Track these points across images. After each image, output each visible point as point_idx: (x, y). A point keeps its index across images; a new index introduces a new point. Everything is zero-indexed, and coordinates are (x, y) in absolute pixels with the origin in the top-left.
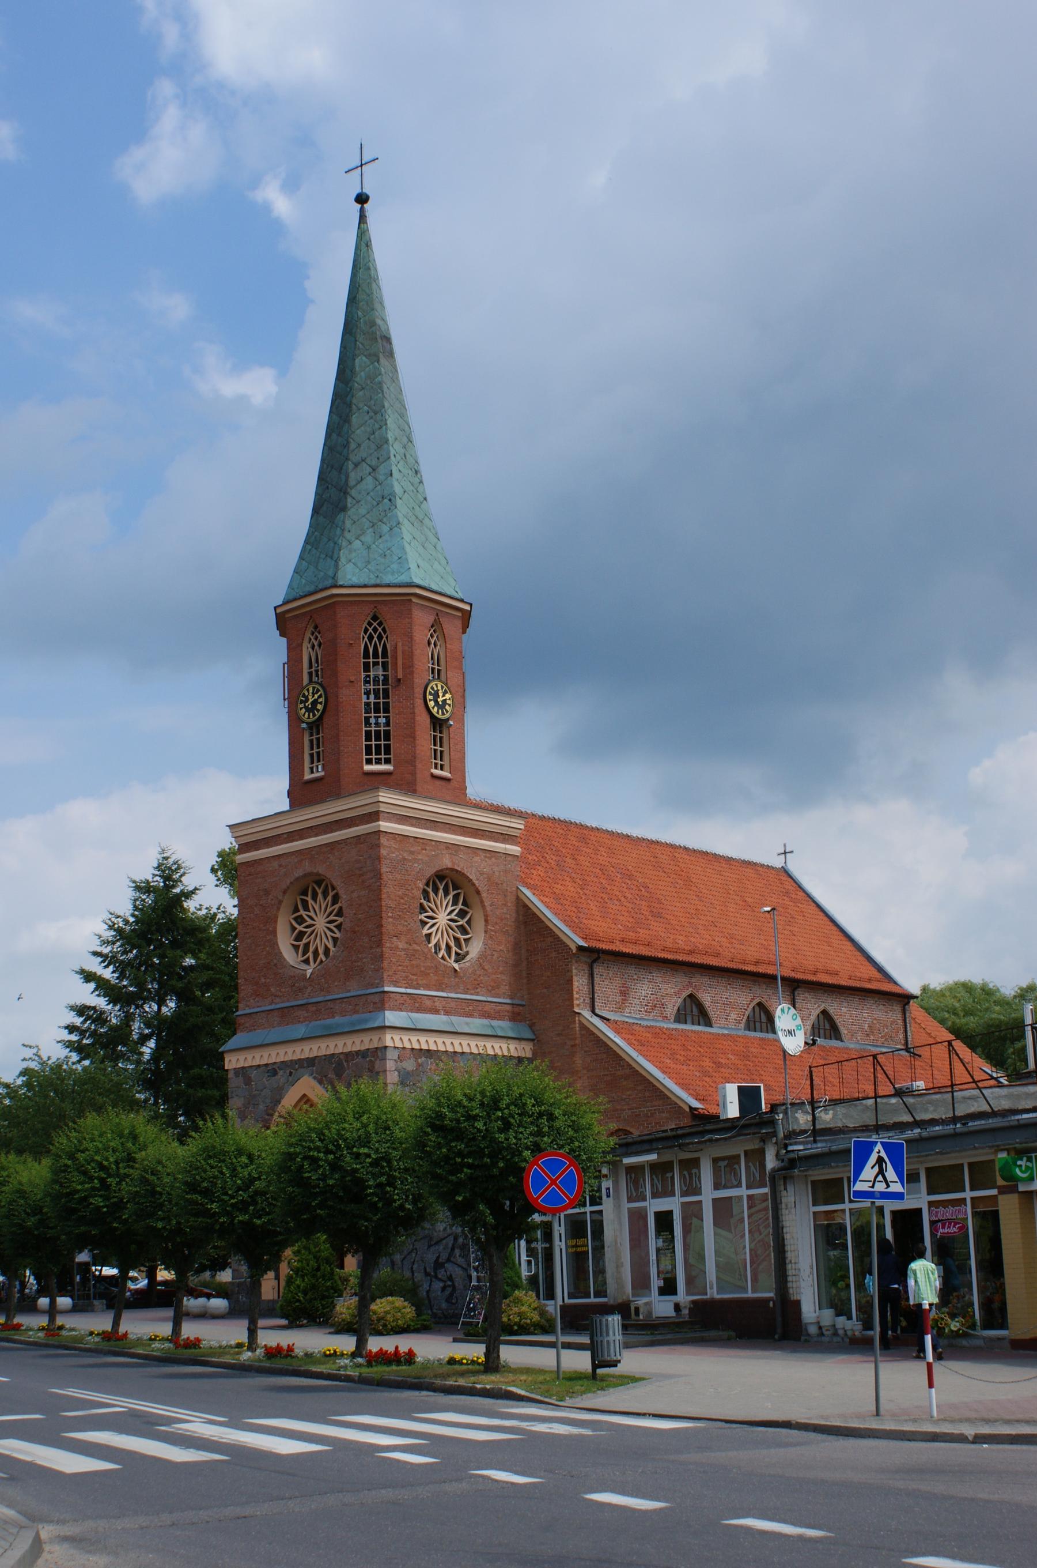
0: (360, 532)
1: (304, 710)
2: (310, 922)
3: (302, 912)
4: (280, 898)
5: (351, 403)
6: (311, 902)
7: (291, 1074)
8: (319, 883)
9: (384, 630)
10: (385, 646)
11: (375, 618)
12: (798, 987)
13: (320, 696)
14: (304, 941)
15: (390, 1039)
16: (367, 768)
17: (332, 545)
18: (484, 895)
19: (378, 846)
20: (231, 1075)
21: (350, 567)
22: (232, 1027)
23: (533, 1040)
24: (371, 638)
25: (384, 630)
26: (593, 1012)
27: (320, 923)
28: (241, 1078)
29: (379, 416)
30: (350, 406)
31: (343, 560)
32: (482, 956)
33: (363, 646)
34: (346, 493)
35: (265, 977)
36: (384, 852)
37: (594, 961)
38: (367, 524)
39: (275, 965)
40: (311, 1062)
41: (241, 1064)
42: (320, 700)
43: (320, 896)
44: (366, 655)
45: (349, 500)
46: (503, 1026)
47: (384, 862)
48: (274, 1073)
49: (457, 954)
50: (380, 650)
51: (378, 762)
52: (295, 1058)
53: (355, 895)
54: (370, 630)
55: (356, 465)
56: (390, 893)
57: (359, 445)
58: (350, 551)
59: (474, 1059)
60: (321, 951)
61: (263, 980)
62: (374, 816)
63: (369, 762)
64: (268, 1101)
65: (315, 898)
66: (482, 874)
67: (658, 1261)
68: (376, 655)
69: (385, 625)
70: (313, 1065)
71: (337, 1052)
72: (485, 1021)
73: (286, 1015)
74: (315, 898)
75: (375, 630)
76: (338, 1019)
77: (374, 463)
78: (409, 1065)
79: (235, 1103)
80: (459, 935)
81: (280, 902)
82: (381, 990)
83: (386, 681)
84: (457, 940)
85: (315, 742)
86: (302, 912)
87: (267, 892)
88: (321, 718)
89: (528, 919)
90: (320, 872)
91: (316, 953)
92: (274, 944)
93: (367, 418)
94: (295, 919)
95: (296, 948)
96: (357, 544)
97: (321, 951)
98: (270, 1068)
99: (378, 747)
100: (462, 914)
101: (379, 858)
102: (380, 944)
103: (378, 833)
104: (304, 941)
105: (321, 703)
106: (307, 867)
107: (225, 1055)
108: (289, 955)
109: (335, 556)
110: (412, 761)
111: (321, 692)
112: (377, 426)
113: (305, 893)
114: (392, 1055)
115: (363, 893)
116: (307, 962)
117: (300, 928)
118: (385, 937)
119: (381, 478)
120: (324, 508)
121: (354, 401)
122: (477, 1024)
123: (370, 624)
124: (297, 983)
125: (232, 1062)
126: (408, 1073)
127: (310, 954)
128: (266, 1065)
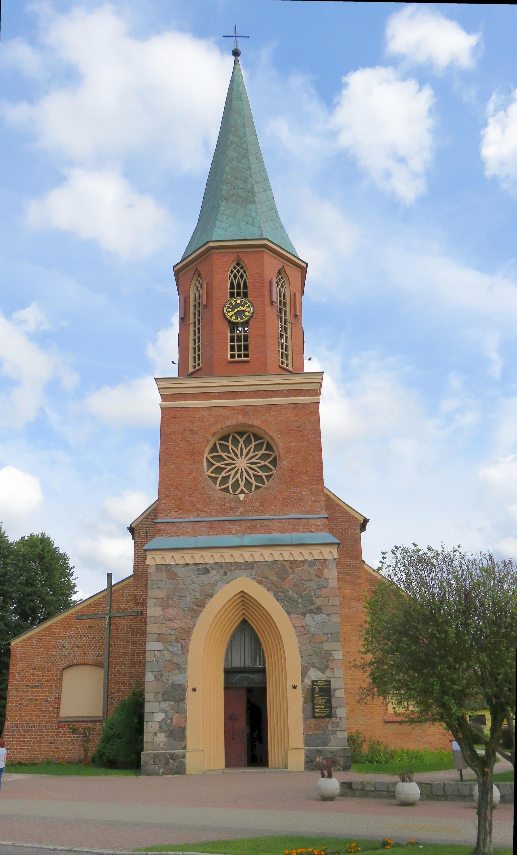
4: (210, 438)
7: (225, 573)
9: (245, 272)
11: (238, 264)
20: (152, 570)
23: (338, 544)
24: (235, 276)
25: (245, 272)
27: (242, 463)
33: (229, 282)
39: (203, 488)
40: (249, 566)
48: (206, 571)
50: (235, 284)
53: (293, 444)
64: (198, 595)
69: (245, 268)
70: (252, 568)
74: (235, 442)
75: (238, 271)
85: (197, 348)
87: (195, 433)
90: (255, 424)
104: (223, 474)
106: (241, 419)
123: (235, 268)
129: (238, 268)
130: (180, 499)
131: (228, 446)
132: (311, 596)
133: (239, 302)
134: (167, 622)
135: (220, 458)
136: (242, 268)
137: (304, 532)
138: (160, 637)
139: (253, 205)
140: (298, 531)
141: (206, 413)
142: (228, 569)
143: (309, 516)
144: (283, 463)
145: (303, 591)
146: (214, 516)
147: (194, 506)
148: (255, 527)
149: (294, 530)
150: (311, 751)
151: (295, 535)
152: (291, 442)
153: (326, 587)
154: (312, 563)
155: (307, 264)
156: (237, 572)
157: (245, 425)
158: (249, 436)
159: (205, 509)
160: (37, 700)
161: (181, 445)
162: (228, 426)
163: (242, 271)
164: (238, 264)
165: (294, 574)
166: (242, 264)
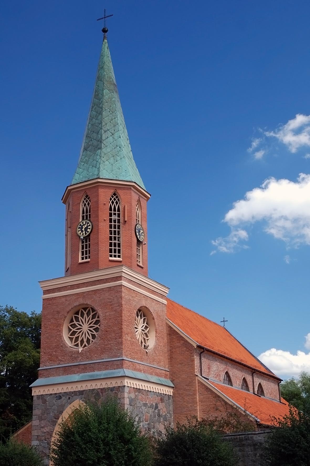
0: (108, 158)
2: (79, 327)
3: (75, 322)
4: (66, 315)
5: (102, 107)
6: (80, 317)
7: (69, 398)
8: (85, 309)
9: (118, 199)
10: (119, 207)
11: (115, 194)
12: (255, 372)
13: (89, 225)
14: (76, 336)
15: (127, 382)
16: (110, 258)
17: (95, 162)
18: (156, 320)
19: (121, 292)
21: (104, 171)
22: (35, 377)
23: (173, 387)
24: (113, 202)
25: (118, 199)
26: (201, 375)
27: (85, 327)
28: (40, 400)
29: (114, 113)
30: (102, 108)
31: (101, 168)
32: (155, 348)
34: (101, 142)
35: (56, 351)
36: (123, 295)
37: (201, 353)
38: (111, 155)
39: (62, 346)
40: (81, 393)
41: (42, 393)
42: (89, 227)
43: (85, 315)
44: (111, 209)
45: (103, 145)
46: (164, 380)
47: (123, 299)
48: (60, 398)
49: (145, 346)
50: (117, 208)
51: (115, 256)
52: (72, 391)
53: (108, 314)
54: (113, 199)
55: (105, 132)
56: (125, 314)
58: (104, 165)
59: (154, 395)
60: (85, 340)
62: (119, 278)
63: (111, 256)
64: (56, 412)
65: (82, 315)
66: (155, 311)
68: (115, 210)
69: (119, 197)
71: (96, 388)
72: (157, 377)
73: (67, 370)
74: (82, 315)
75: (115, 199)
76: (96, 373)
77: (113, 132)
78: (133, 396)
79: (36, 412)
80: (145, 337)
81: (65, 317)
82: (122, 358)
83: (119, 221)
84: (144, 339)
85: (85, 246)
86: (75, 322)
87: (58, 312)
88: (89, 235)
89: (172, 333)
90: (88, 303)
91: (82, 341)
92: (61, 337)
93: (109, 114)
94: (71, 326)
95: (71, 339)
96: (107, 163)
97: (85, 340)
98: (57, 395)
100: (146, 327)
101: (121, 297)
102: (121, 337)
103: (121, 286)
104: (76, 336)
105: (90, 229)
106: (81, 301)
107: (32, 389)
108: (68, 343)
109: (98, 166)
110: (131, 257)
111: (90, 223)
112: (113, 117)
113: (77, 313)
114: (126, 390)
115: (112, 313)
116: (77, 345)
117: (73, 330)
118: (123, 334)
119: (116, 138)
120: (90, 148)
121: (104, 106)
122: (154, 379)
124: (74, 356)
125: (35, 392)
126: (132, 399)
127: (79, 342)
128: (56, 394)
130: (51, 355)
134: (42, 429)
136: (117, 197)
138: (38, 438)
141: (63, 299)
142: (71, 396)
143: (113, 359)
146: (66, 364)
147: (57, 358)
148: (86, 368)
152: (106, 313)
154: (112, 389)
156: (75, 397)
163: (117, 199)
164: (115, 194)
165: (103, 396)
166: (117, 195)
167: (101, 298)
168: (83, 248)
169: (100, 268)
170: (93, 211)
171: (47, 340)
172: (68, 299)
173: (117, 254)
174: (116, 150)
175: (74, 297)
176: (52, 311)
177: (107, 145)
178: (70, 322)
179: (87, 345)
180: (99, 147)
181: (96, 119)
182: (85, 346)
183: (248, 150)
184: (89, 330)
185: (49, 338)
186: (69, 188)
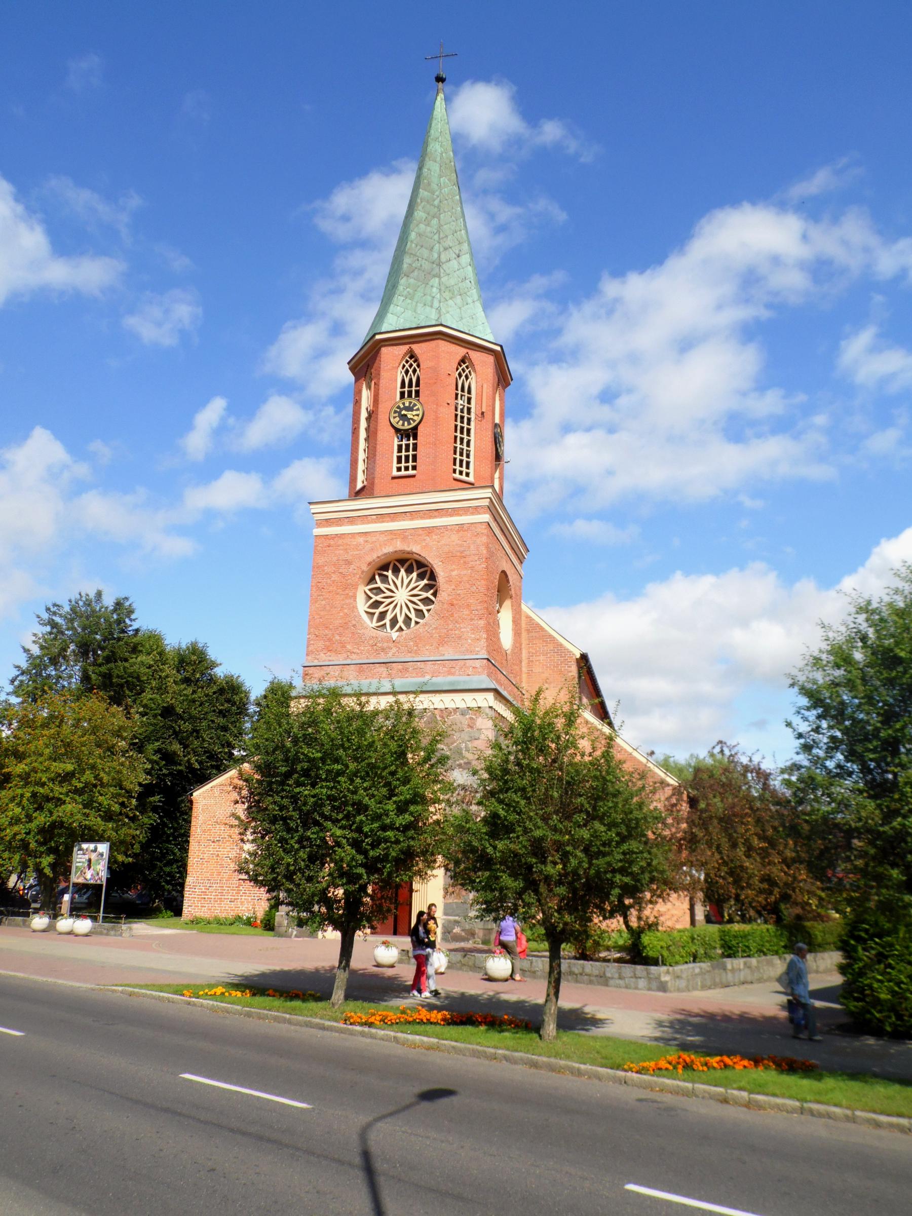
1: (398, 419)
9: (418, 366)
24: (407, 372)
25: (418, 366)
27: (402, 596)
35: (340, 635)
39: (354, 626)
53: (455, 573)
57: (447, 236)
61: (337, 637)
67: (767, 1095)
68: (410, 385)
75: (411, 366)
87: (348, 563)
90: (414, 550)
91: (394, 621)
96: (451, 302)
97: (401, 619)
99: (407, 457)
106: (399, 546)
129: (411, 361)
130: (330, 640)
131: (387, 577)
132: (461, 749)
133: (407, 404)
135: (378, 591)
137: (460, 675)
139: (437, 280)
140: (453, 674)
141: (361, 540)
144: (443, 595)
145: (452, 744)
148: (407, 670)
149: (450, 673)
150: (449, 921)
151: (451, 678)
152: (452, 571)
153: (478, 739)
155: (501, 346)
157: (403, 552)
158: (411, 565)
159: (355, 651)
160: (218, 856)
161: (335, 577)
162: (385, 554)
163: (467, 371)
164: (411, 357)
167: (443, 542)
168: (400, 450)
169: (376, 492)
170: (426, 383)
171: (322, 613)
172: (369, 538)
173: (464, 469)
174: (464, 284)
175: (382, 538)
176: (336, 558)
177: (448, 272)
178: (368, 584)
179: (404, 627)
180: (434, 273)
181: (428, 225)
182: (401, 629)
183: (342, 200)
184: (392, 597)
185: (328, 608)
186: (378, 337)
